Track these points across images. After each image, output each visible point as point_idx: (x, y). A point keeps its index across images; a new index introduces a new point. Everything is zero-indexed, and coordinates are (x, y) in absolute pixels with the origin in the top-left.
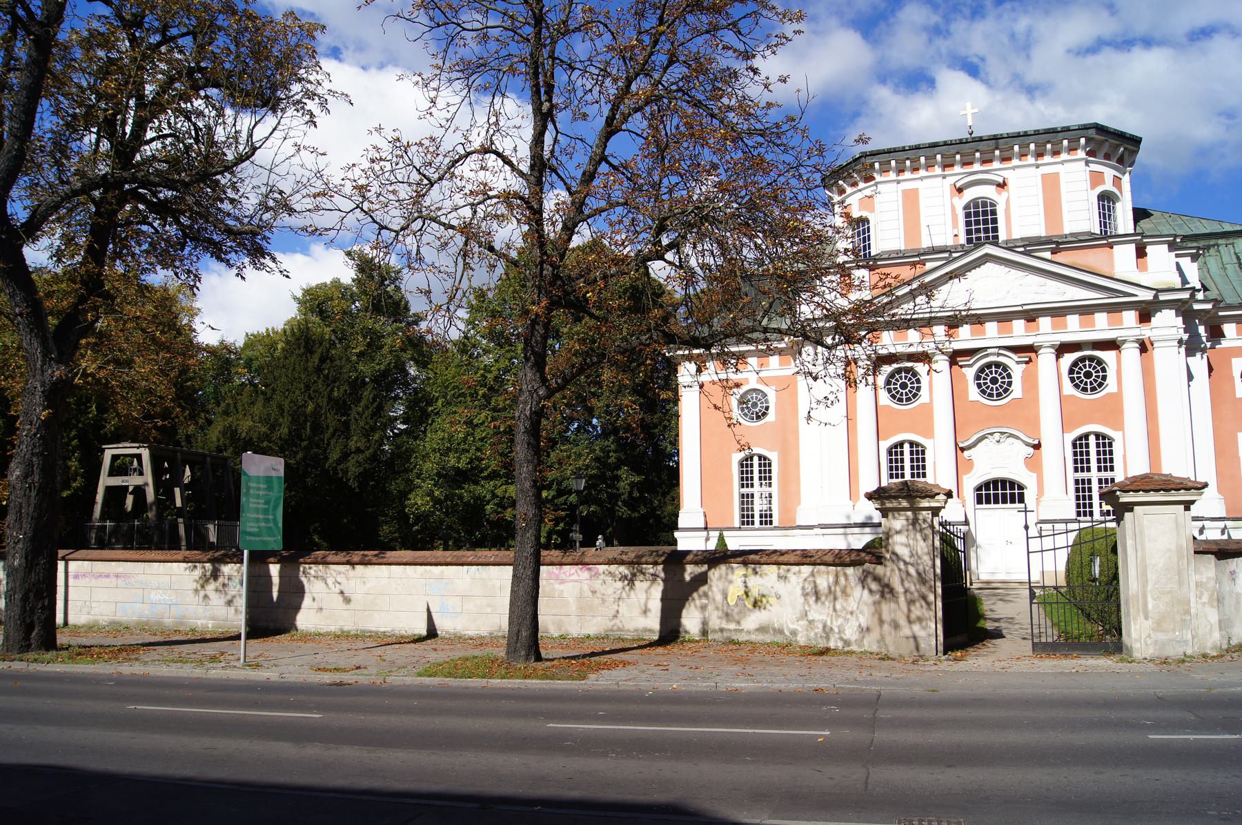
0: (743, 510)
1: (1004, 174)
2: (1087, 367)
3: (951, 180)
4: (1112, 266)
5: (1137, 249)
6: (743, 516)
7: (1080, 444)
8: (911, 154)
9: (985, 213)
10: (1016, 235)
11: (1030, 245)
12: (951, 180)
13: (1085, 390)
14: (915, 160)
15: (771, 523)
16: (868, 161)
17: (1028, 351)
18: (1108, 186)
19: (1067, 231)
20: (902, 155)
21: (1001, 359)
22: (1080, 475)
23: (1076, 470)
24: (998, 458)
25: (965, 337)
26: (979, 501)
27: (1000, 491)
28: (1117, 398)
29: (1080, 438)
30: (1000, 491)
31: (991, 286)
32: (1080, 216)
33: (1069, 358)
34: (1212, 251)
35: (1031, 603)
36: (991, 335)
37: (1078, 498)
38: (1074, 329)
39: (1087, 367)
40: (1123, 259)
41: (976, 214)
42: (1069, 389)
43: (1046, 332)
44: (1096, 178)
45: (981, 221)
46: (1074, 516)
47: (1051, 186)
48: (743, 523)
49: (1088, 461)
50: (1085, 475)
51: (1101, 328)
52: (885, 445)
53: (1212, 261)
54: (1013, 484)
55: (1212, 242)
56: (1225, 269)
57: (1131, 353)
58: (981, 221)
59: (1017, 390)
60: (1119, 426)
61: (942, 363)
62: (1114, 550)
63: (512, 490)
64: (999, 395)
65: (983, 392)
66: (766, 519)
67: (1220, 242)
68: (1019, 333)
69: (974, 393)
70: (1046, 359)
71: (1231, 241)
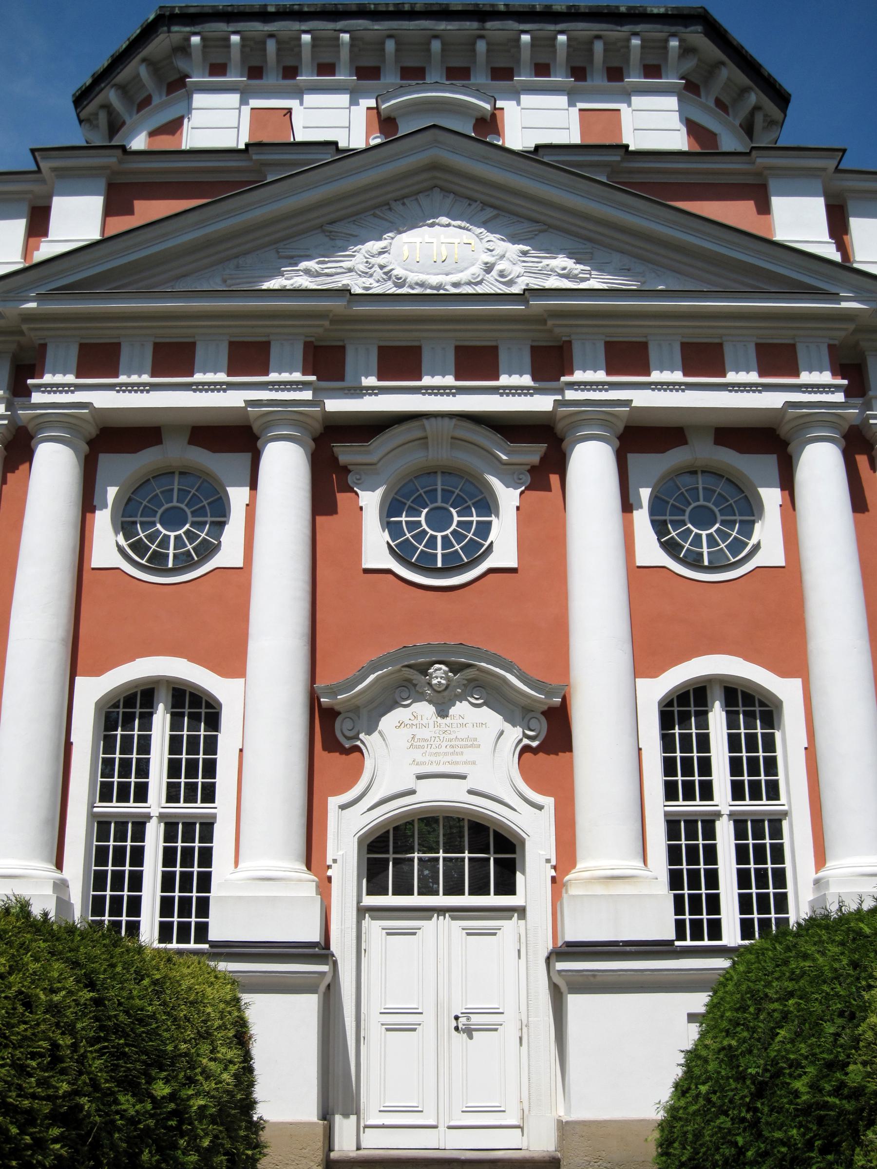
4: (770, 227)
7: (682, 710)
21: (464, 459)
23: (670, 792)
24: (439, 754)
26: (374, 875)
28: (788, 580)
30: (448, 856)
36: (438, 395)
38: (665, 392)
51: (742, 393)
52: (91, 691)
60: (794, 661)
61: (284, 464)
62: (130, 500)
68: (516, 395)
69: (376, 549)
70: (591, 464)
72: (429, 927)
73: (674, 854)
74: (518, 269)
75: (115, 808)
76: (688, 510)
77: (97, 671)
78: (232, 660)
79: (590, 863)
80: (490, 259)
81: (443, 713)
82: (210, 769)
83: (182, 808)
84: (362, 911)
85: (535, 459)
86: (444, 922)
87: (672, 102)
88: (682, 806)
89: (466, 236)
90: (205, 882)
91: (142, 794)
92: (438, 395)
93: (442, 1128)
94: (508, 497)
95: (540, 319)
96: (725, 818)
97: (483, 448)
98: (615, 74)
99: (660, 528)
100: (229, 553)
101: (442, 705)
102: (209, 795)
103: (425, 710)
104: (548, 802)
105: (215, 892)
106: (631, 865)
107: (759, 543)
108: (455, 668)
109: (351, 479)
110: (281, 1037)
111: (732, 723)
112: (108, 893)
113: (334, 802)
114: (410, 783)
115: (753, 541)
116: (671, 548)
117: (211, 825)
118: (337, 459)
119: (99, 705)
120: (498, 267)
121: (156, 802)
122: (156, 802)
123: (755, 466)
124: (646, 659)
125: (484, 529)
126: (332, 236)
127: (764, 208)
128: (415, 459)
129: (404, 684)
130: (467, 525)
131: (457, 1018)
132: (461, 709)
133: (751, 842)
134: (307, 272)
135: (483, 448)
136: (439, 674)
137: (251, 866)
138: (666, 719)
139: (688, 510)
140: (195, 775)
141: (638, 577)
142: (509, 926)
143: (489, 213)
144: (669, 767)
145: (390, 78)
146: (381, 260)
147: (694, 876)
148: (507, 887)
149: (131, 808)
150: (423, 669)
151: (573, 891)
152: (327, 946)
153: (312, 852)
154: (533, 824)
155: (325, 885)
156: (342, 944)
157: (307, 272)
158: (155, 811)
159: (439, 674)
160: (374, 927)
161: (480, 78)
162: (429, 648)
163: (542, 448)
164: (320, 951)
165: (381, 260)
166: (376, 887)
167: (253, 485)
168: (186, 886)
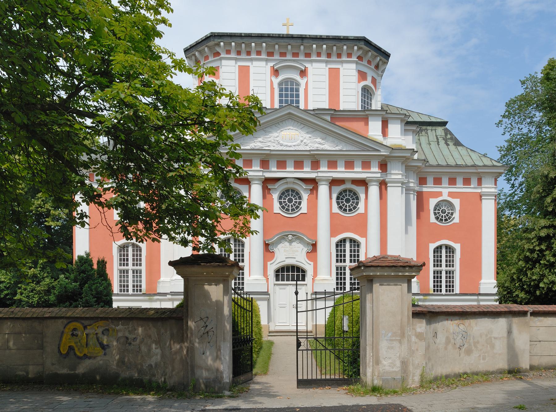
0: (120, 281)
1: (307, 65)
2: (348, 195)
3: (271, 64)
4: (368, 132)
5: (383, 121)
6: (121, 286)
7: (341, 243)
8: (246, 40)
9: (292, 90)
10: (310, 107)
11: (318, 113)
12: (271, 64)
13: (345, 210)
14: (248, 45)
15: (141, 291)
16: (217, 40)
17: (313, 183)
18: (368, 82)
19: (341, 109)
20: (240, 40)
21: (296, 187)
22: (339, 264)
23: (337, 261)
24: (290, 253)
25: (274, 172)
26: (277, 278)
27: (291, 273)
28: (364, 217)
29: (341, 241)
30: (291, 273)
31: (289, 138)
32: (350, 100)
33: (337, 190)
34: (423, 133)
35: (297, 350)
36: (290, 172)
37: (337, 279)
38: (341, 172)
39: (348, 195)
40: (374, 129)
41: (287, 90)
42: (336, 209)
43: (324, 172)
44: (362, 76)
45: (289, 92)
47: (334, 76)
48: (121, 291)
49: (127, 260)
50: (342, 264)
51: (358, 173)
53: (423, 139)
55: (424, 128)
56: (430, 144)
57: (374, 190)
58: (289, 92)
59: (304, 208)
60: (364, 234)
63: (528, 254)
64: (293, 210)
65: (283, 207)
66: (137, 288)
67: (429, 128)
68: (307, 172)
69: (277, 208)
70: (323, 189)
71: (434, 128)
73: (337, 274)
74: (309, 142)
79: (319, 277)
80: (302, 139)
81: (290, 245)
82: (141, 260)
85: (312, 188)
87: (354, 66)
89: (297, 133)
90: (243, 279)
92: (290, 172)
94: (305, 196)
95: (314, 155)
98: (339, 56)
99: (338, 203)
101: (291, 242)
102: (140, 265)
103: (287, 244)
104: (312, 263)
105: (245, 281)
106: (328, 277)
108: (293, 235)
109: (271, 192)
110: (262, 306)
111: (351, 247)
113: (269, 263)
114: (285, 259)
116: (340, 208)
120: (304, 141)
123: (360, 191)
124: (333, 233)
125: (300, 203)
126: (265, 132)
127: (367, 124)
128: (285, 187)
129: (283, 238)
130: (296, 202)
132: (294, 244)
134: (260, 142)
136: (290, 237)
137: (253, 277)
138: (337, 246)
141: (333, 216)
143: (302, 126)
144: (337, 256)
145: (276, 57)
146: (277, 139)
147: (341, 278)
148: (303, 280)
150: (287, 236)
151: (316, 282)
152: (268, 292)
153: (265, 274)
154: (308, 267)
155: (267, 281)
157: (260, 142)
159: (290, 237)
160: (277, 288)
161: (301, 57)
162: (288, 232)
163: (313, 183)
164: (267, 293)
165: (277, 139)
166: (277, 280)
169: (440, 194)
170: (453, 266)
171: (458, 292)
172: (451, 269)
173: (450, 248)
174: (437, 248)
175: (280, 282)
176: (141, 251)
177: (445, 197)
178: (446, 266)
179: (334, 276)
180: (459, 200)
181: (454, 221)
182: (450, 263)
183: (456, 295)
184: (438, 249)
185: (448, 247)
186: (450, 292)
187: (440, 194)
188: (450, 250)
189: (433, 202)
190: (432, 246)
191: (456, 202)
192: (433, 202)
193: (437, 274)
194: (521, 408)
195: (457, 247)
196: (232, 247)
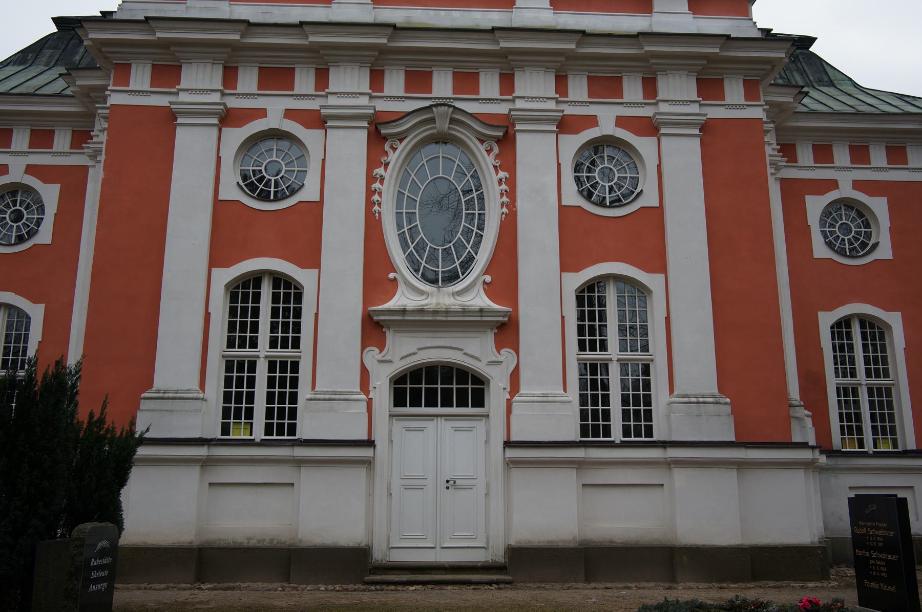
26: (399, 400)
46: (573, 434)
52: (224, 276)
54: (463, 374)
72: (431, 425)
75: (237, 352)
76: (837, 225)
77: (227, 264)
78: (311, 257)
82: (297, 328)
83: (279, 352)
84: (392, 416)
86: (441, 422)
88: (589, 355)
91: (254, 344)
93: (438, 548)
96: (615, 363)
97: (491, 126)
100: (309, 193)
102: (296, 344)
107: (642, 190)
112: (233, 405)
115: (638, 190)
117: (298, 363)
118: (380, 132)
119: (227, 286)
121: (264, 349)
122: (264, 349)
131: (448, 481)
133: (641, 392)
135: (491, 126)
138: (580, 301)
139: (837, 225)
140: (288, 330)
142: (480, 425)
149: (247, 352)
156: (380, 437)
158: (262, 354)
160: (398, 425)
167: (218, 204)
168: (282, 400)
169: (833, 185)
170: (886, 375)
171: (912, 445)
172: (882, 381)
173: (872, 326)
174: (838, 324)
175: (408, 410)
176: (299, 298)
177: (846, 191)
178: (868, 375)
179: (573, 394)
180: (885, 199)
181: (877, 255)
182: (878, 364)
183: (906, 454)
184: (841, 328)
185: (866, 322)
186: (638, 434)
187: (833, 185)
188: (874, 331)
189: (815, 206)
190: (826, 320)
191: (879, 206)
192: (815, 206)
193: (847, 394)
194: (450, 610)
195: (894, 320)
196: (847, 247)
